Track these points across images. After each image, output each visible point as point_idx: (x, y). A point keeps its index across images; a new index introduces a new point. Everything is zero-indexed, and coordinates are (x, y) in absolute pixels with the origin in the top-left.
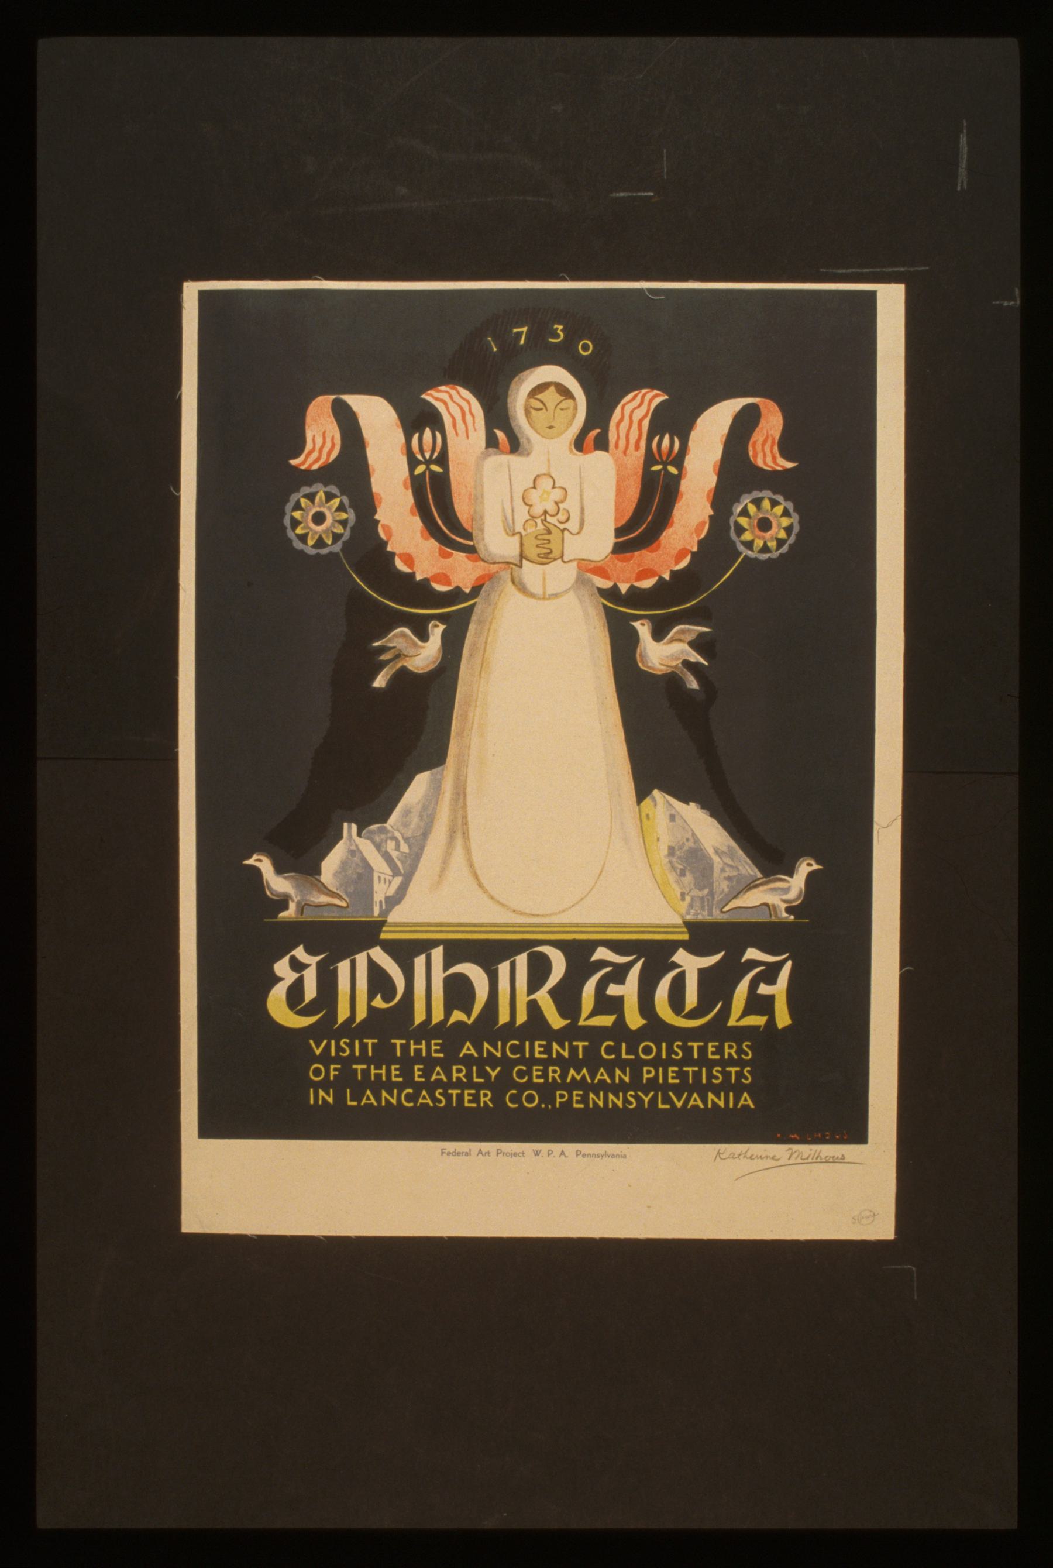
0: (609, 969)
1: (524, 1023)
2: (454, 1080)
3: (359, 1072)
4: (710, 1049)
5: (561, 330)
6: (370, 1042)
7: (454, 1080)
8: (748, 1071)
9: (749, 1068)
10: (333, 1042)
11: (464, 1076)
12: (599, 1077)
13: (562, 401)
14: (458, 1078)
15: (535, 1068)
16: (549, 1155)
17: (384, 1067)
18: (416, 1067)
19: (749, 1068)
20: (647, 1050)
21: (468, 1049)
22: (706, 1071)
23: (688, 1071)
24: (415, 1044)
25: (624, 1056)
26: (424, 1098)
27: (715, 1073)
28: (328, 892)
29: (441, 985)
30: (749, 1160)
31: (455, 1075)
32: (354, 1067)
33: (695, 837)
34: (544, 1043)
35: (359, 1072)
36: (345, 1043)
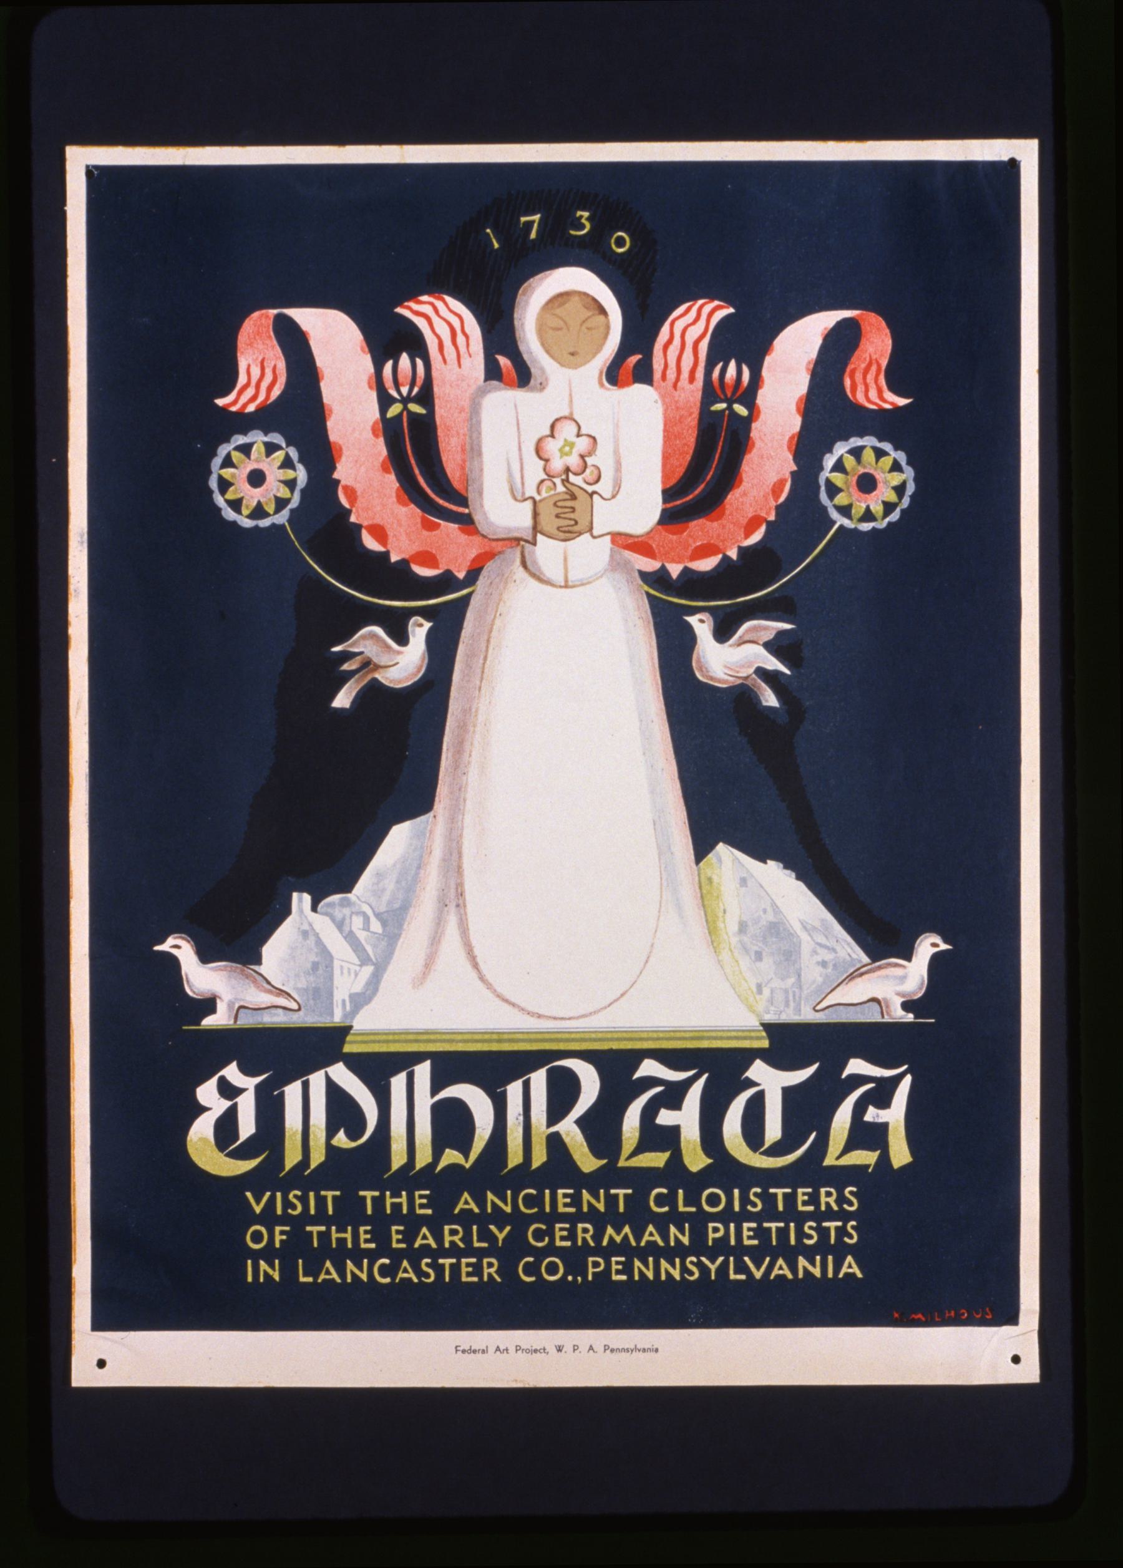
2: (447, 1245)
4: (801, 1198)
6: (330, 1194)
14: (452, 1243)
16: (574, 1350)
18: (394, 1228)
20: (713, 1200)
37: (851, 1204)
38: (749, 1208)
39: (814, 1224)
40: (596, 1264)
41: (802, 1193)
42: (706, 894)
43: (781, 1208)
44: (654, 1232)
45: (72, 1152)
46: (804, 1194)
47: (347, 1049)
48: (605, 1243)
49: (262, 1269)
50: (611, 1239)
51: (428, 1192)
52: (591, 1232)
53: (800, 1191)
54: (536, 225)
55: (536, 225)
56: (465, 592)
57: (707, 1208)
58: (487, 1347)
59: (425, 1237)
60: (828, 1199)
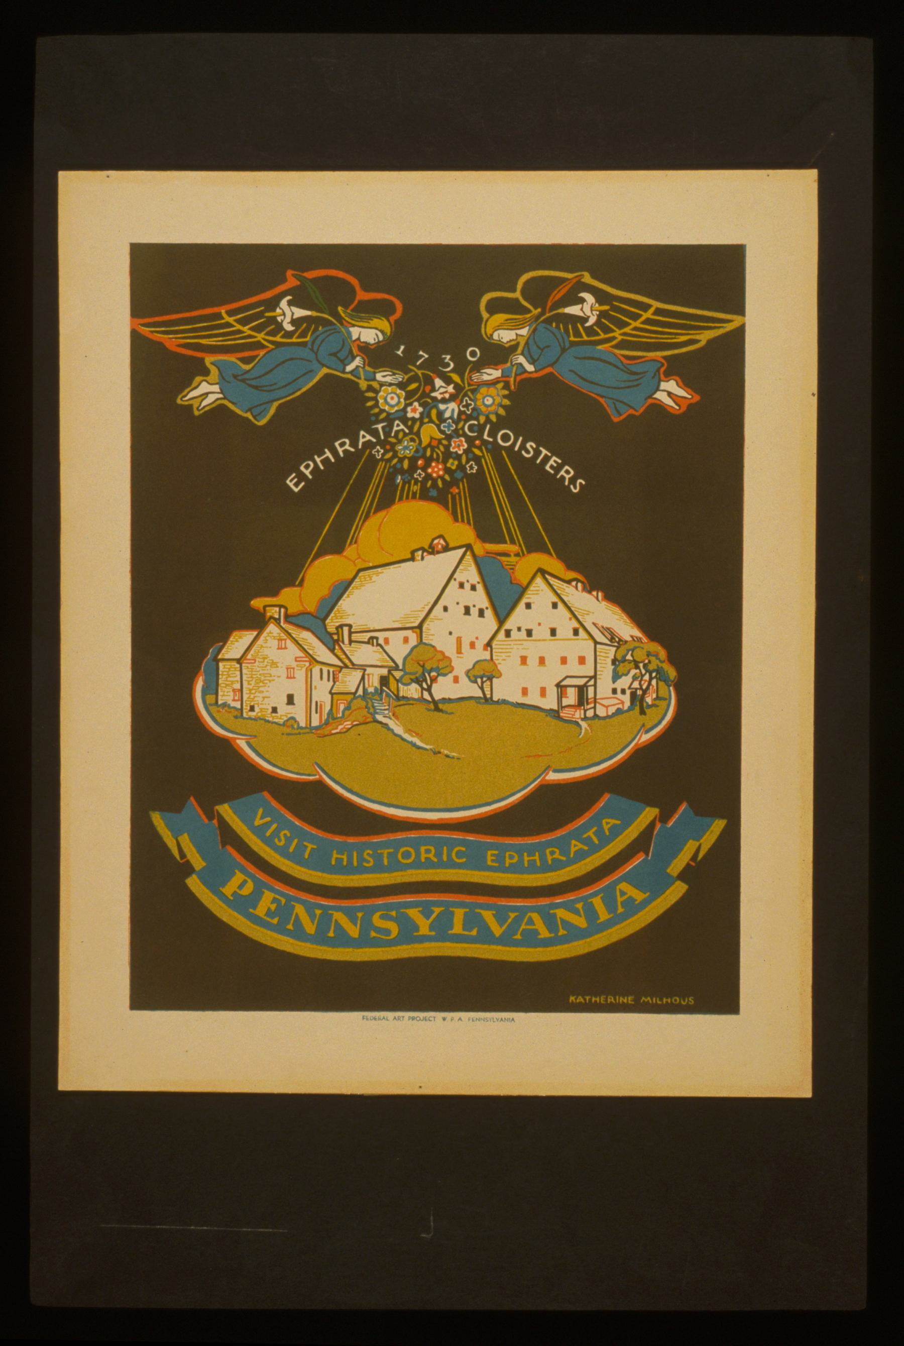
2: (342, 455)
3: (530, 858)
4: (551, 462)
7: (342, 455)
8: (581, 484)
9: (583, 483)
11: (435, 856)
13: (357, 549)
14: (345, 451)
19: (583, 483)
25: (485, 437)
26: (575, 846)
28: (500, 327)
30: (424, 1021)
33: (674, 397)
35: (530, 858)
39: (534, 446)
40: (511, 857)
42: (346, 557)
44: (365, 434)
45: (194, 687)
46: (555, 461)
47: (458, 471)
48: (268, 819)
49: (262, 822)
53: (554, 458)
56: (450, 509)
58: (374, 582)
59: (364, 437)
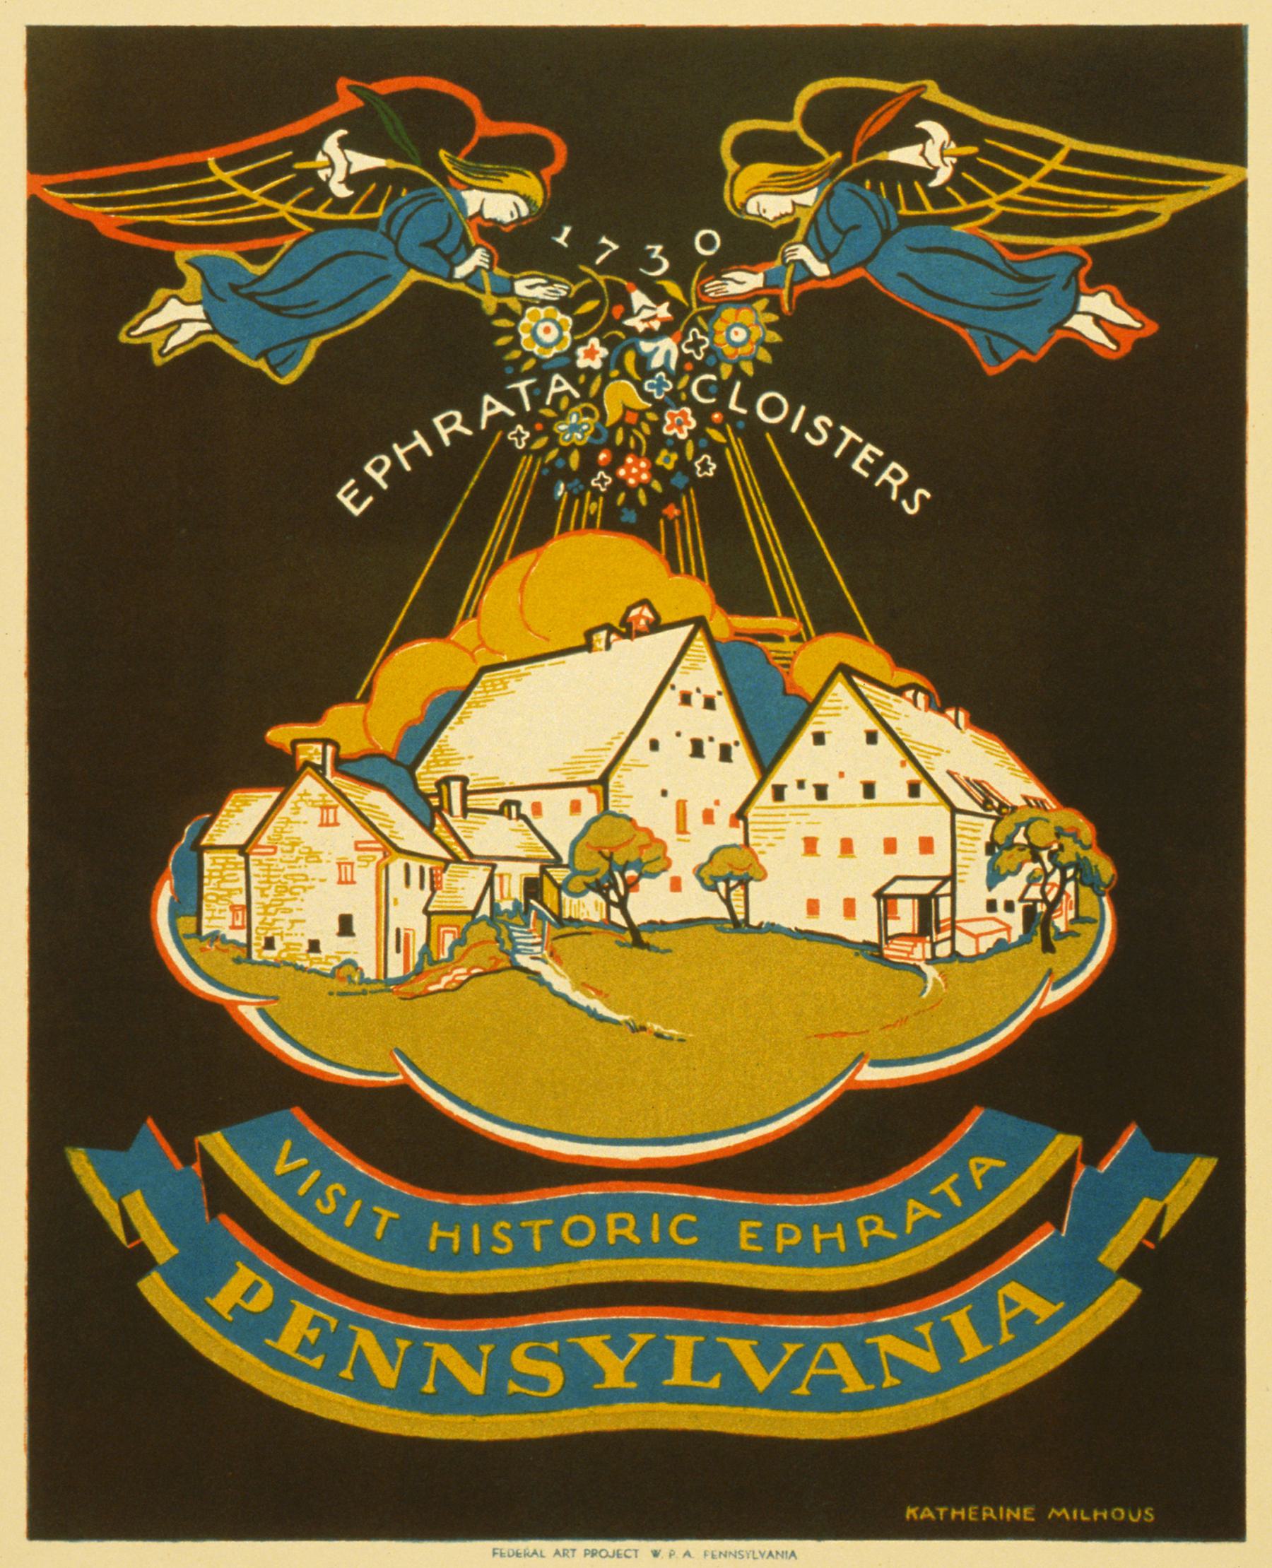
0: (687, 304)
1: (778, 333)
2: (447, 442)
4: (864, 455)
5: (662, 253)
10: (315, 1175)
12: (486, 414)
15: (340, 496)
17: (385, 486)
20: (772, 407)
21: (979, 1166)
22: (806, 413)
23: (822, 1241)
24: (822, 1232)
27: (496, 1233)
29: (753, 1357)
31: (444, 433)
32: (416, 433)
34: (880, 453)
36: (336, 1192)
37: (911, 505)
38: (808, 436)
41: (869, 452)
43: (958, 1202)
46: (871, 454)
50: (653, 250)
51: (352, 482)
52: (632, 1223)
53: (869, 447)
54: (608, 252)
55: (608, 252)
56: (663, 548)
57: (761, 414)
58: (513, 692)
60: (891, 480)
